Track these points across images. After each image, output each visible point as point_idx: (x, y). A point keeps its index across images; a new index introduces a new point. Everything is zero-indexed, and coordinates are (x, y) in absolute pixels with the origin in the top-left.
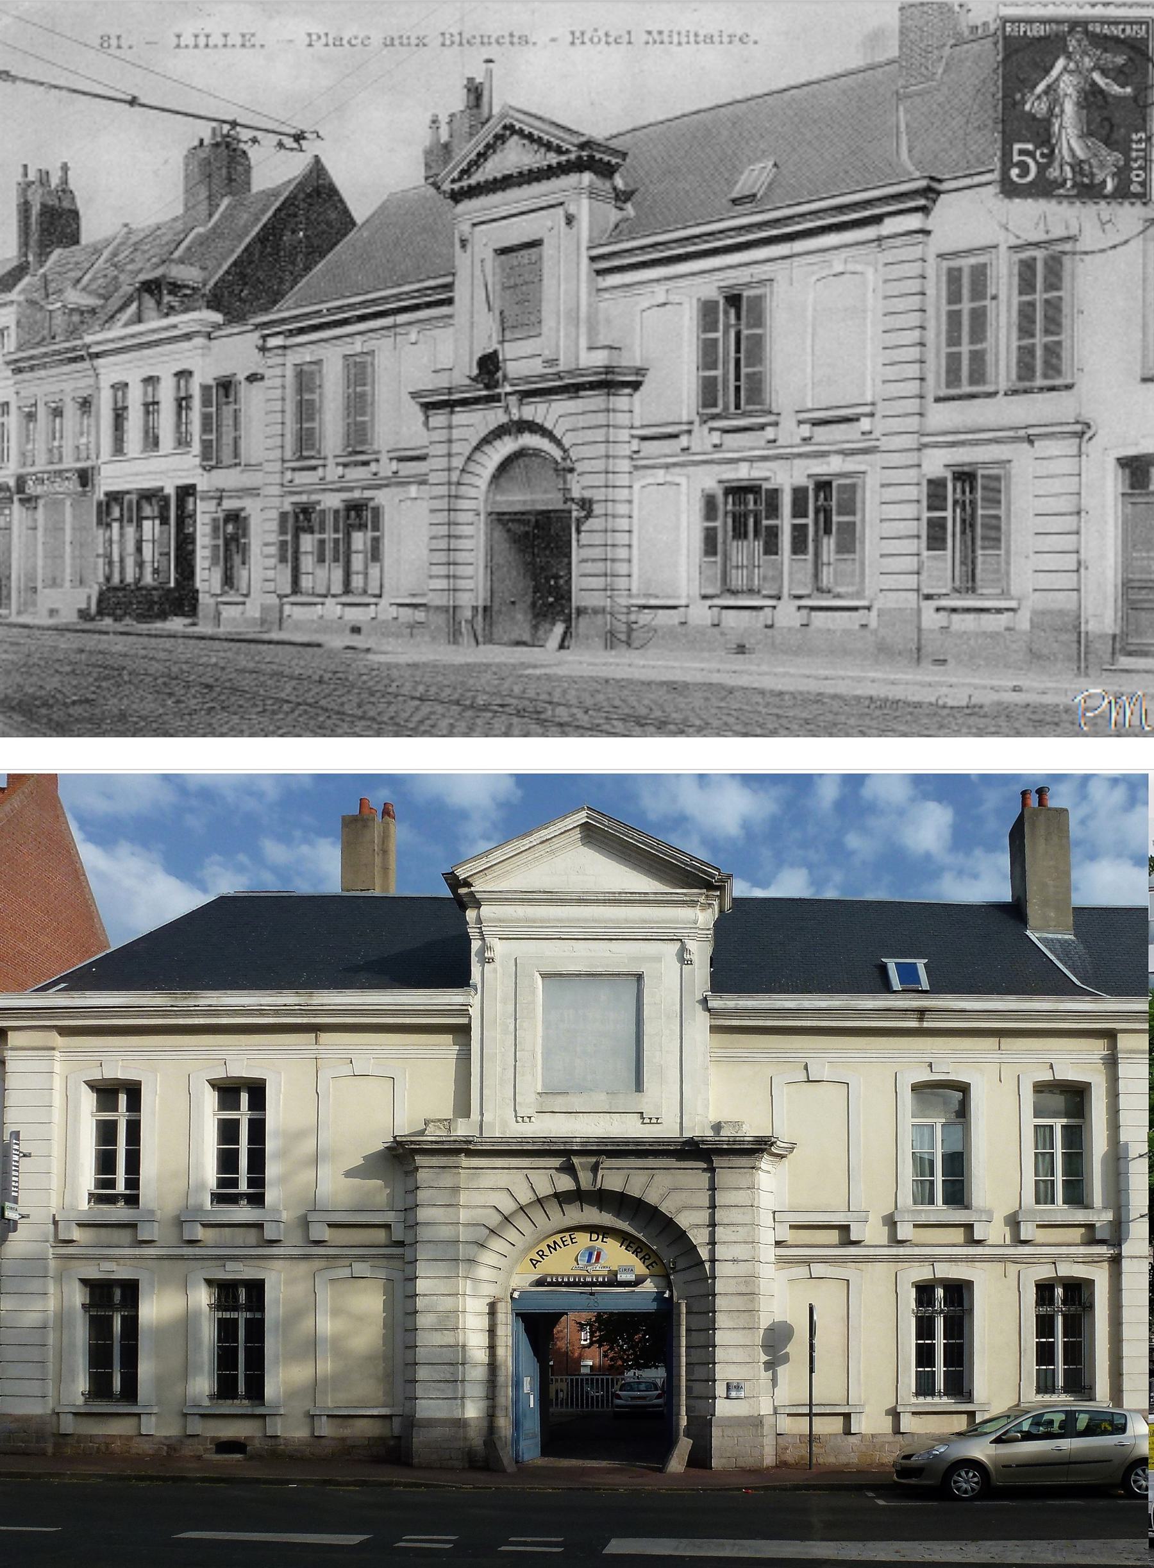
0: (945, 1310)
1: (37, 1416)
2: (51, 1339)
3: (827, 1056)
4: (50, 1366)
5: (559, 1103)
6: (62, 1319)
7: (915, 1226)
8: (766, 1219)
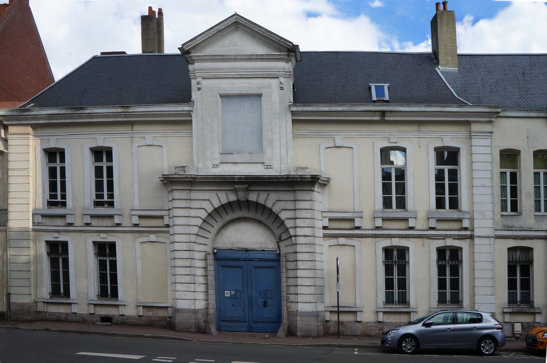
0: (396, 261)
1: (27, 303)
2: (32, 268)
3: (342, 135)
4: (32, 280)
5: (229, 158)
6: (37, 259)
7: (383, 220)
8: (318, 215)
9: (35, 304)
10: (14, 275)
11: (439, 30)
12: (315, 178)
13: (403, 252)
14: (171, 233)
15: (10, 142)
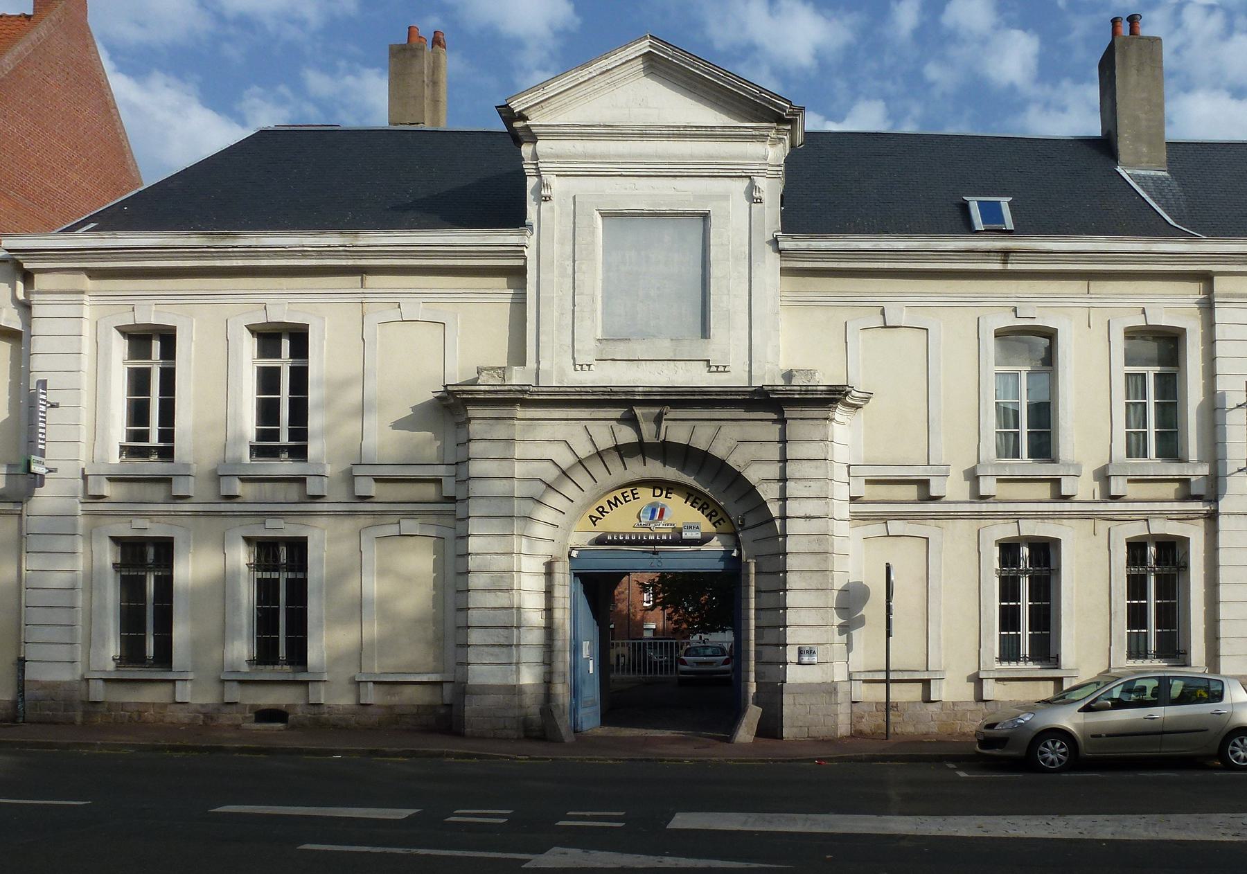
0: (1030, 571)
1: (65, 683)
2: (80, 601)
3: (905, 300)
5: (620, 350)
6: (92, 579)
8: (840, 473)
9: (84, 684)
10: (36, 616)
11: (1118, 81)
12: (840, 392)
13: (1045, 551)
14: (460, 514)
15: (37, 311)
